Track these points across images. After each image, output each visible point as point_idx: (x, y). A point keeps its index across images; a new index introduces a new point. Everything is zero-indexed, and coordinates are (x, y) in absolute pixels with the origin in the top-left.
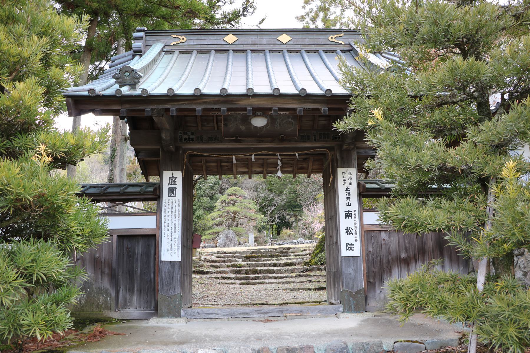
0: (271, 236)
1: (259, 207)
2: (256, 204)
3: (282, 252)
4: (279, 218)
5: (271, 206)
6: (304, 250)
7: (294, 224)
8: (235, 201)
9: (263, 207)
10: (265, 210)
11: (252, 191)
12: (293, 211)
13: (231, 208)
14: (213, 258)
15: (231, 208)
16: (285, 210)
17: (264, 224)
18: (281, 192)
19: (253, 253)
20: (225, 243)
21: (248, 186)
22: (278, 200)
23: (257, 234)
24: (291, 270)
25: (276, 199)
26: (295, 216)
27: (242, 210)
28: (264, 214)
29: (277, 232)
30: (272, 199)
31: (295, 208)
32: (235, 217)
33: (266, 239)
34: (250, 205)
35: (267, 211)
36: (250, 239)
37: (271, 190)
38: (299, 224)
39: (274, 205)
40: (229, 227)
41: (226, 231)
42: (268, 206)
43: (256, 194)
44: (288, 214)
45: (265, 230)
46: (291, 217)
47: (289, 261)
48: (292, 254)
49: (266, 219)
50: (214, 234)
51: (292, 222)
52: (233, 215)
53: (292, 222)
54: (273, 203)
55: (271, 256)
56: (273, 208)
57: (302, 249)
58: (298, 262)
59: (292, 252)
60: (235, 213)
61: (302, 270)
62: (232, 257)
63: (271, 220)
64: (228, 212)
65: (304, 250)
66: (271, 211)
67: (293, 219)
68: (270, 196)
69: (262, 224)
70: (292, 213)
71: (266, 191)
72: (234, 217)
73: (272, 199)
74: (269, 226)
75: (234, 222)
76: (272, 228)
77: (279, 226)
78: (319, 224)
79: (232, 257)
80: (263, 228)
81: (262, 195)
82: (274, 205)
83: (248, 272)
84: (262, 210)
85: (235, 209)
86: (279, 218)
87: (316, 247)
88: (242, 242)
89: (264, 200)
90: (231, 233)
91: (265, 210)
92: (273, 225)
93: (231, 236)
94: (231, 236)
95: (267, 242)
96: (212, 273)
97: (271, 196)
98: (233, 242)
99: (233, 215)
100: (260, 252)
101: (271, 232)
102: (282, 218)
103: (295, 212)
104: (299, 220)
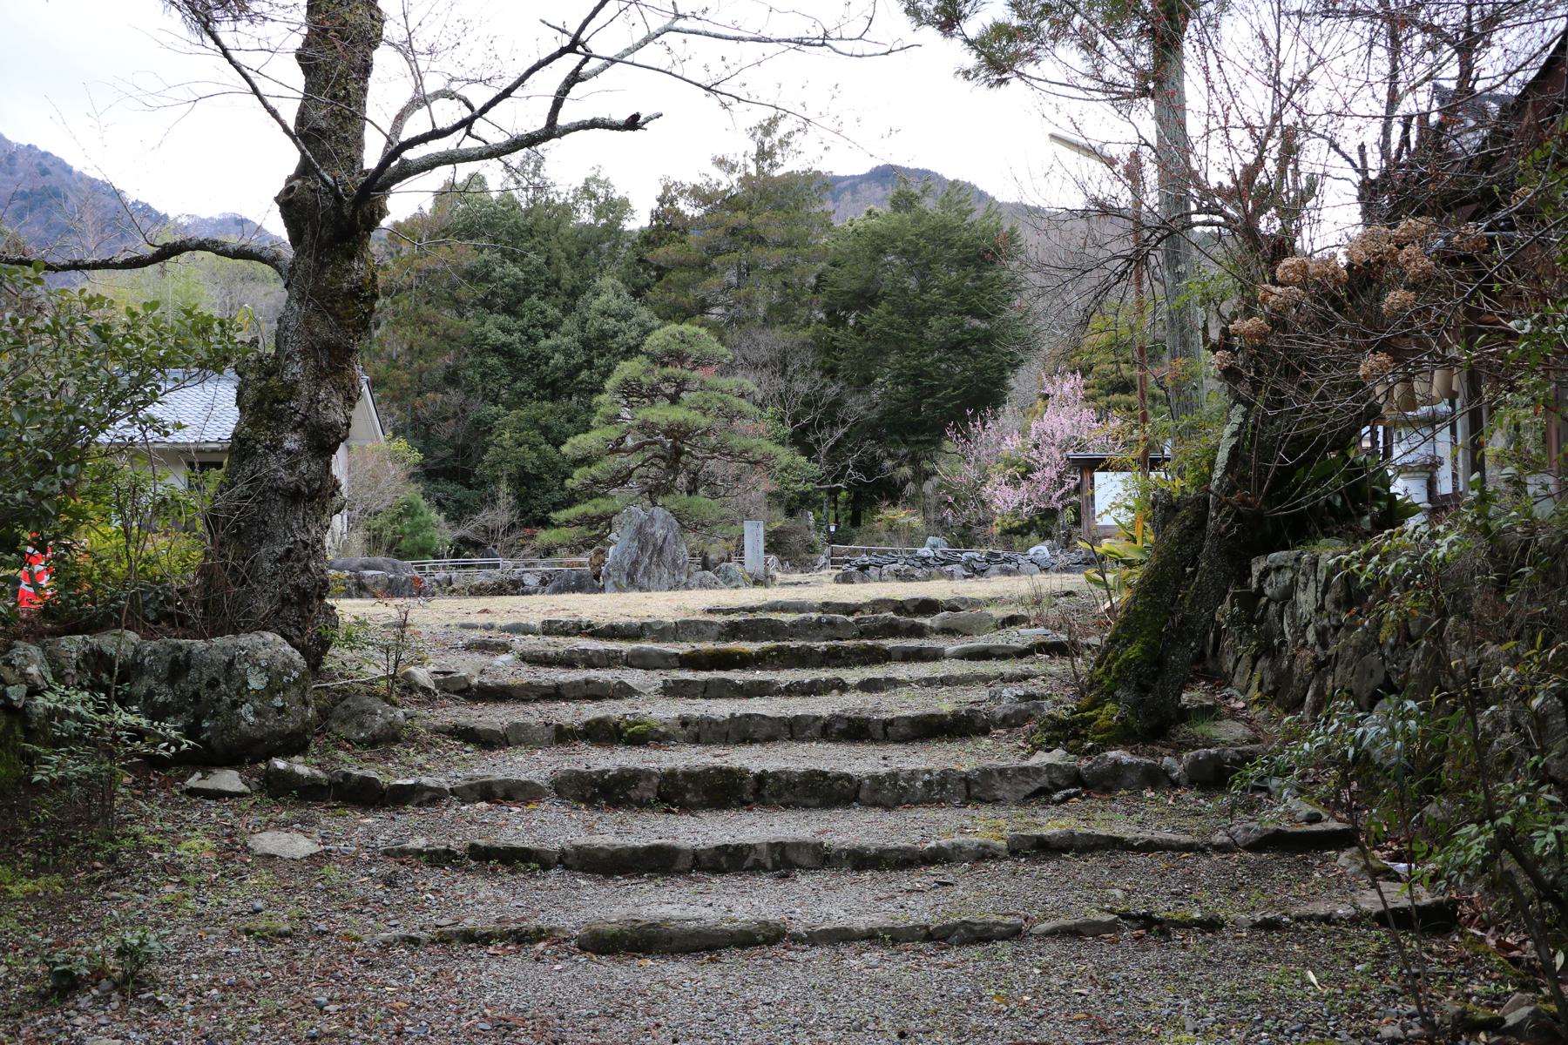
0: (833, 529)
1: (790, 430)
2: (782, 420)
3: (892, 630)
4: (858, 467)
5: (833, 424)
6: (1012, 621)
7: (910, 488)
8: (681, 385)
9: (804, 430)
10: (811, 439)
11: (767, 372)
12: (905, 442)
13: (662, 413)
14: (504, 669)
15: (662, 413)
16: (880, 439)
17: (809, 487)
18: (868, 380)
19: (733, 631)
20: (635, 563)
21: (754, 356)
22: (857, 406)
23: (780, 521)
24: (966, 780)
25: (850, 401)
26: (914, 461)
27: (704, 422)
28: (808, 451)
29: (850, 513)
30: (837, 403)
31: (915, 432)
32: (679, 452)
33: (815, 537)
34: (743, 401)
35: (817, 441)
36: (747, 542)
37: (831, 372)
38: (928, 487)
39: (844, 422)
40: (655, 492)
41: (639, 512)
42: (821, 426)
43: (780, 383)
44: (891, 456)
45: (810, 508)
46: (900, 465)
47: (945, 704)
48: (951, 645)
49: (815, 469)
50: (589, 521)
51: (904, 482)
52: (668, 443)
53: (904, 482)
54: (840, 415)
55: (833, 658)
56: (839, 432)
57: (998, 613)
58: (999, 711)
59: (948, 631)
60: (678, 433)
61: (1043, 780)
62: (609, 660)
63: (830, 473)
64: (646, 427)
65: (1012, 621)
66: (831, 442)
67: (906, 471)
68: (828, 391)
69: (800, 487)
70: (903, 451)
71: (817, 375)
72: (674, 450)
73: (837, 403)
74: (823, 494)
75: (677, 472)
76: (835, 501)
77: (858, 496)
78: (1009, 490)
79: (609, 660)
80: (806, 501)
81: (801, 387)
82: (844, 422)
83: (681, 791)
84: (801, 440)
85: (677, 414)
86: (858, 467)
87: (1125, 625)
88: (713, 557)
89: (808, 403)
90: (661, 524)
91: (811, 439)
92: (839, 490)
93: (660, 533)
94: (660, 533)
95: (820, 547)
96: (432, 797)
97: (832, 391)
98: (667, 557)
99: (668, 443)
100: (774, 630)
101: (832, 513)
102: (869, 466)
103: (915, 448)
104: (928, 475)
